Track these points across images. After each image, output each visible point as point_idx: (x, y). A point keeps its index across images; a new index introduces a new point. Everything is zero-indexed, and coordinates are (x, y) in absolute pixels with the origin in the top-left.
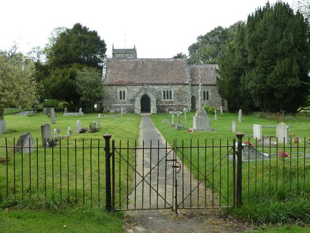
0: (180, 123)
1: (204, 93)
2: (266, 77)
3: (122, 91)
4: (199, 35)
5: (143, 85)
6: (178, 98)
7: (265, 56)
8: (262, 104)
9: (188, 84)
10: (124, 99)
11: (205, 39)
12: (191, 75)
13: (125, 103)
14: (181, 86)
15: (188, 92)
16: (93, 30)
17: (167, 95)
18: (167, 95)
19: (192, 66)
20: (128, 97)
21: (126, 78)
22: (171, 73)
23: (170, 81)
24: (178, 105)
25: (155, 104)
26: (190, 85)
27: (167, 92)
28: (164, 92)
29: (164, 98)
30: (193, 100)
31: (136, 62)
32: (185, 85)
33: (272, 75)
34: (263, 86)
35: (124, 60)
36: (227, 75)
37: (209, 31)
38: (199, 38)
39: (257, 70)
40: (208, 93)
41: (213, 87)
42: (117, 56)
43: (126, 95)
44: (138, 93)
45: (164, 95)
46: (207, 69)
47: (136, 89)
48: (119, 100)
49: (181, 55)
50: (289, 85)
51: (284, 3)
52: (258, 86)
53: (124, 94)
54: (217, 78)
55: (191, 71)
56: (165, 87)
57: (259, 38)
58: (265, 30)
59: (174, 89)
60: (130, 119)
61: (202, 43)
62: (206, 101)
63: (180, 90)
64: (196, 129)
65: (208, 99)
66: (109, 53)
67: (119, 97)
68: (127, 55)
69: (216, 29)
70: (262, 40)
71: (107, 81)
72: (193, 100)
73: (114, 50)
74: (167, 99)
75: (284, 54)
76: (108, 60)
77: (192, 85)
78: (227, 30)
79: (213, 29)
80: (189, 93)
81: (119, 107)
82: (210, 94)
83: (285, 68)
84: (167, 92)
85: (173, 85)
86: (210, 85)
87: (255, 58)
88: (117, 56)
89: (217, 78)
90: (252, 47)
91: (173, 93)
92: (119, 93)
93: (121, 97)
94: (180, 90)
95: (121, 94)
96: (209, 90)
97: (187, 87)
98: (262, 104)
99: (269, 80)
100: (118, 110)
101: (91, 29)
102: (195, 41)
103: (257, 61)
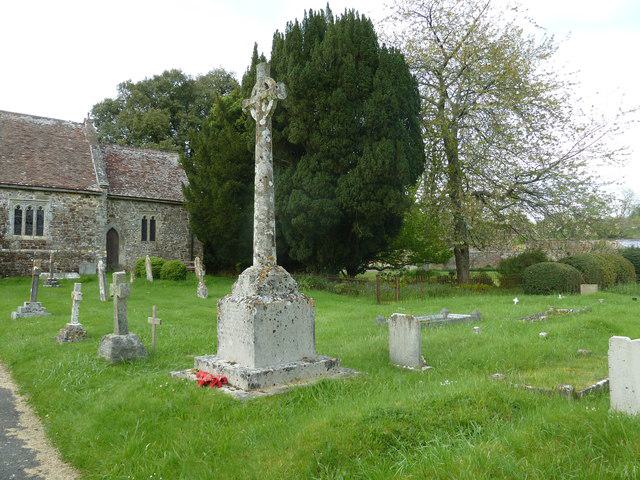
0: (123, 329)
1: (144, 221)
2: (335, 184)
4: (124, 79)
6: (65, 233)
7: (335, 128)
8: (315, 254)
9: (97, 195)
11: (142, 93)
12: (107, 171)
14: (75, 198)
18: (29, 222)
19: (108, 148)
22: (43, 158)
23: (40, 180)
26: (104, 198)
27: (29, 210)
28: (18, 212)
29: (18, 231)
30: (112, 239)
32: (87, 196)
33: (352, 177)
34: (329, 206)
36: (218, 175)
38: (122, 86)
39: (313, 163)
40: (153, 222)
41: (169, 208)
45: (18, 222)
46: (150, 162)
50: (391, 205)
52: (316, 204)
55: (106, 159)
56: (20, 196)
57: (320, 80)
58: (334, 63)
59: (52, 206)
60: (178, 295)
61: (132, 102)
62: (149, 245)
63: (72, 210)
64: (253, 369)
65: (153, 238)
69: (166, 74)
70: (329, 87)
72: (112, 239)
74: (29, 233)
75: (378, 130)
77: (111, 198)
78: (192, 82)
79: (160, 73)
80: (102, 220)
82: (159, 225)
83: (384, 163)
84: (29, 210)
85: (51, 192)
86: (160, 202)
87: (309, 131)
90: (303, 103)
91: (48, 216)
94: (72, 210)
96: (158, 215)
97: (94, 201)
98: (315, 254)
99: (344, 192)
102: (114, 95)
103: (316, 138)
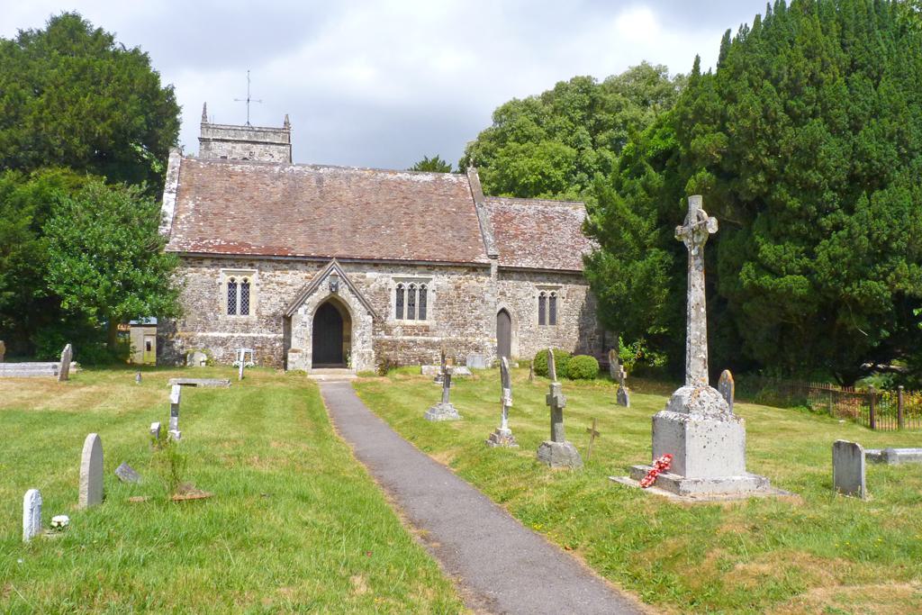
3: (239, 280)
5: (322, 262)
6: (450, 316)
10: (245, 311)
13: (247, 327)
15: (488, 297)
16: (130, 47)
17: (412, 305)
18: (412, 305)
20: (260, 304)
21: (256, 232)
22: (423, 225)
24: (450, 341)
25: (368, 336)
27: (412, 290)
28: (400, 291)
29: (400, 315)
31: (295, 178)
35: (248, 167)
37: (522, 97)
42: (219, 149)
43: (253, 299)
44: (300, 300)
45: (400, 304)
46: (548, 219)
47: (296, 278)
48: (224, 316)
49: (657, 74)
51: (444, 163)
53: (246, 295)
54: (586, 219)
65: (553, 321)
66: (188, 134)
67: (224, 304)
68: (257, 149)
71: (173, 245)
73: (205, 126)
74: (411, 317)
76: (187, 164)
81: (223, 343)
88: (219, 149)
89: (586, 219)
92: (224, 289)
93: (232, 303)
94: (457, 288)
95: (232, 295)
100: (218, 352)
101: (125, 40)
